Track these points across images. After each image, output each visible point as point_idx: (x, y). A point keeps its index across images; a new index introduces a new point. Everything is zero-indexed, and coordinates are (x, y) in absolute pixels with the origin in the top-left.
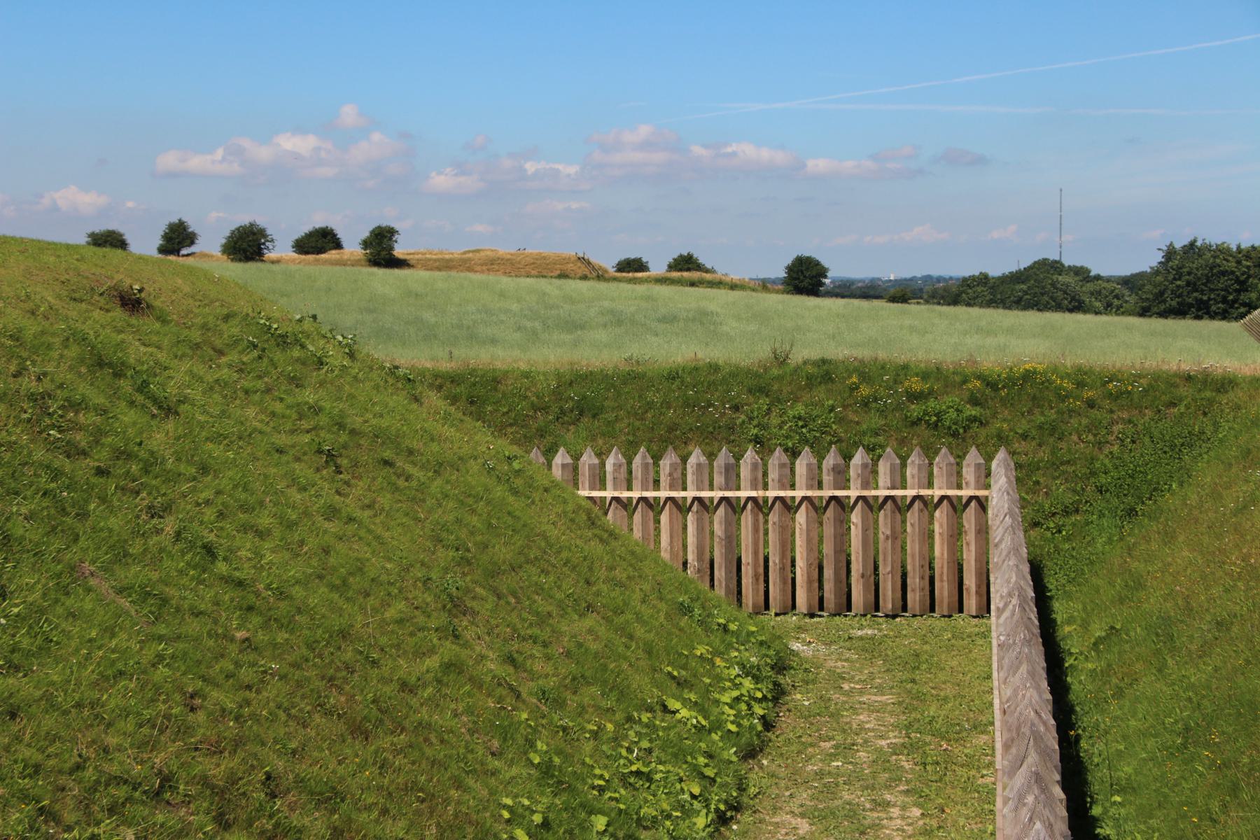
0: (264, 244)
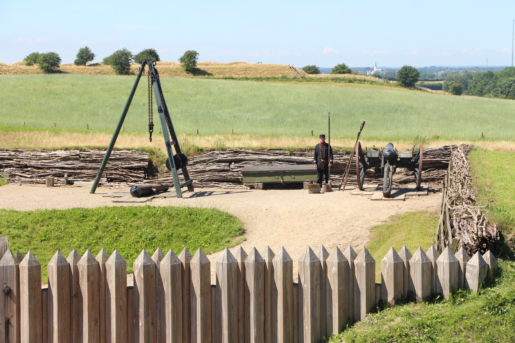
0: (130, 60)
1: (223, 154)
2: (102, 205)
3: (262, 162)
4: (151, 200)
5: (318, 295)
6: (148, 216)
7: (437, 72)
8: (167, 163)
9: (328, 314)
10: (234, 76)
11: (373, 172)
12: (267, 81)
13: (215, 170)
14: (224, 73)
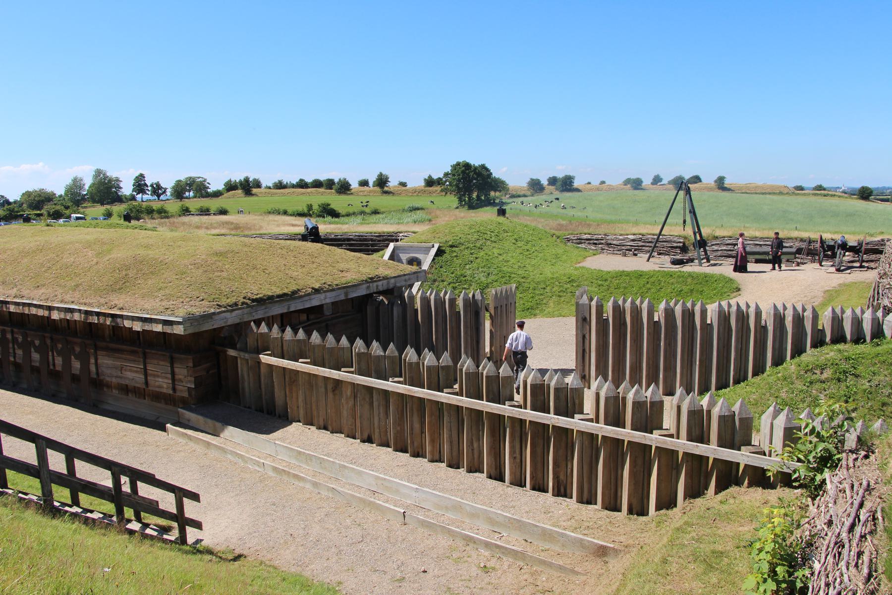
2: (652, 269)
4: (682, 267)
5: (778, 334)
6: (679, 277)
8: (694, 244)
9: (784, 346)
10: (748, 191)
13: (725, 250)
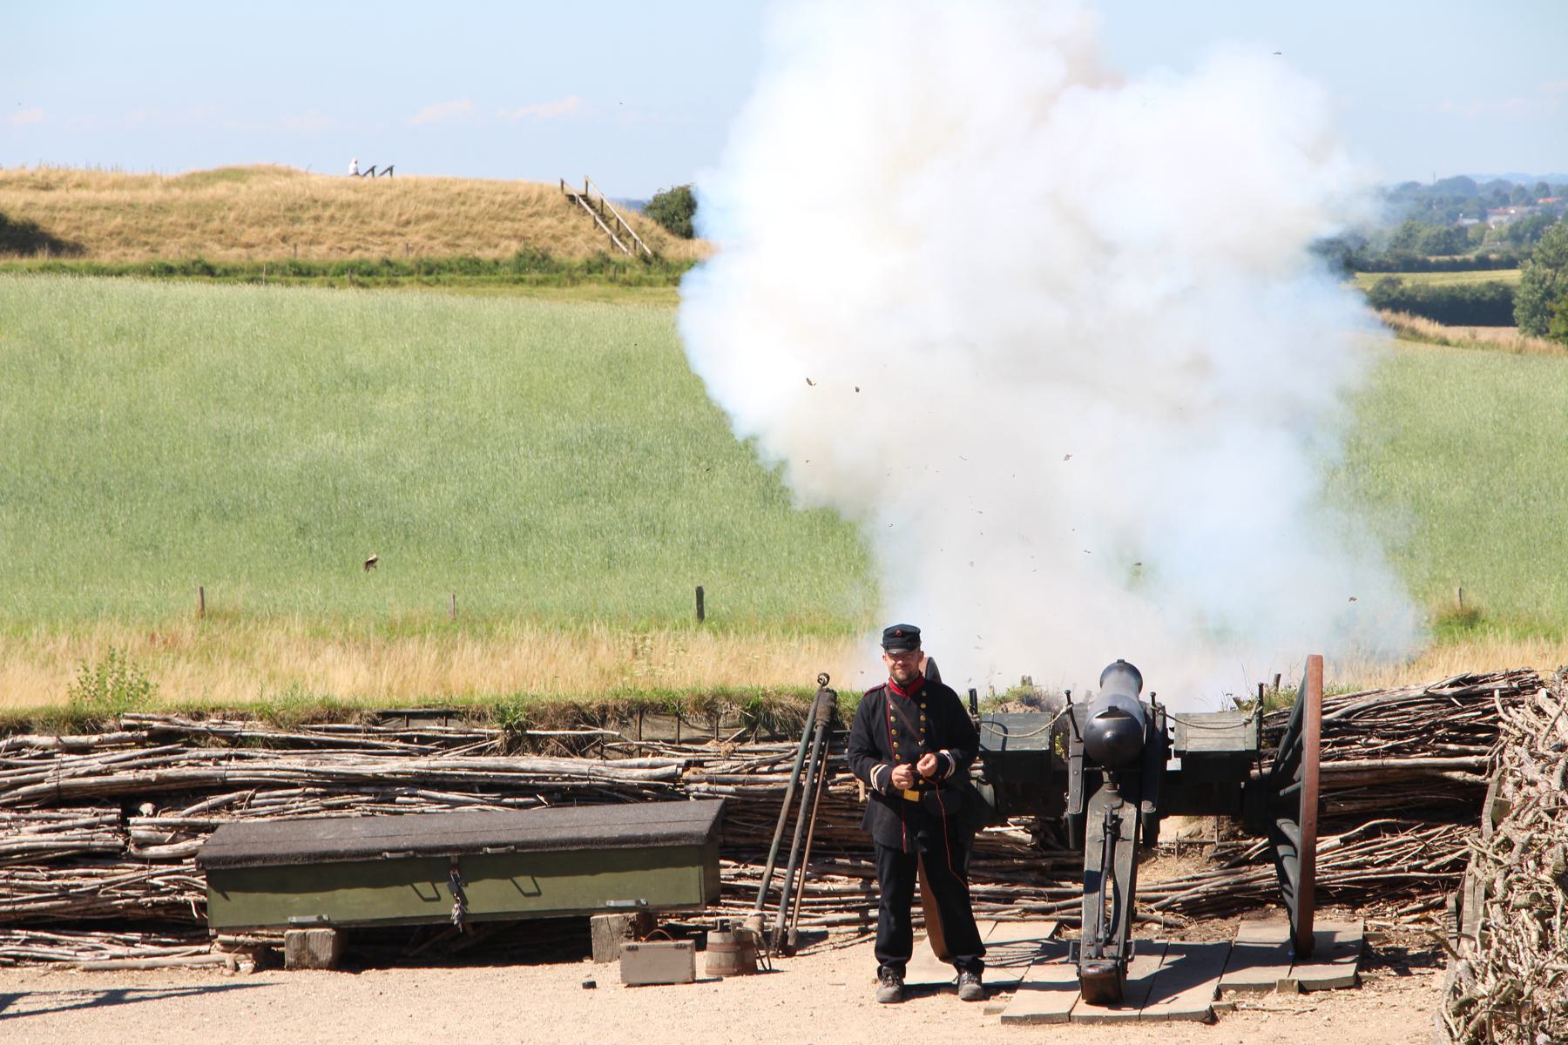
1: (84, 750)
3: (331, 795)
7: (1483, 216)
10: (217, 254)
11: (1021, 843)
12: (428, 284)
13: (34, 857)
14: (152, 239)
